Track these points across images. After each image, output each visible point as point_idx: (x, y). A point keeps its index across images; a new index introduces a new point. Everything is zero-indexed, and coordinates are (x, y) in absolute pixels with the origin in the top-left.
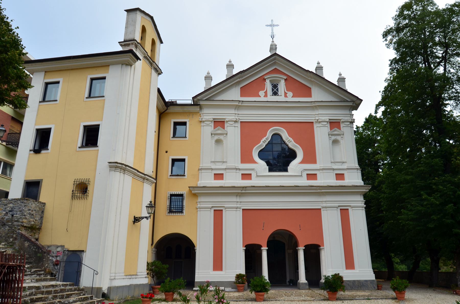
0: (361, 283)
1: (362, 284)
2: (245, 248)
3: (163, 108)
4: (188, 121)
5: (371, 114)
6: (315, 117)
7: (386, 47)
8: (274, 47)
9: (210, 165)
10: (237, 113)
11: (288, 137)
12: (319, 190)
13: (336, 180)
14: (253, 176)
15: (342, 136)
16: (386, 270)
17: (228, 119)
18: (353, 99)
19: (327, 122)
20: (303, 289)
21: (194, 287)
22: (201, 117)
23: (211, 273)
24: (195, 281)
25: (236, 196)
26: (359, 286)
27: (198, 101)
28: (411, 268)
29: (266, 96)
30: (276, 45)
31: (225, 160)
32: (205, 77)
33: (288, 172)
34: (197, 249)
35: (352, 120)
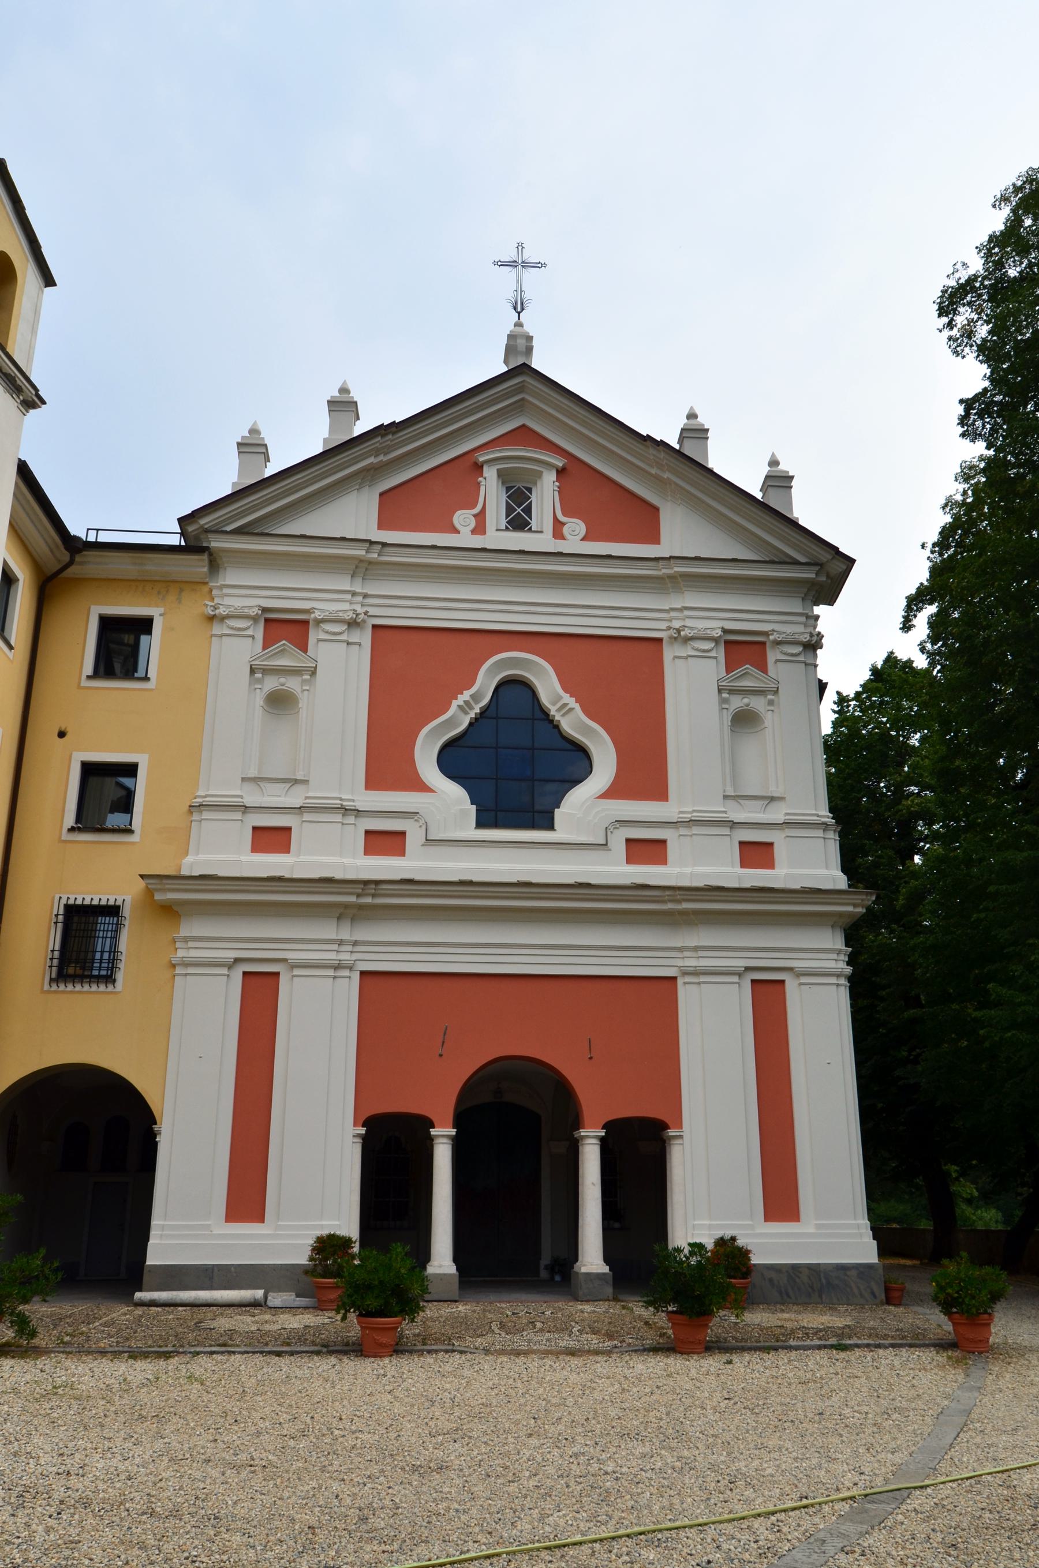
0: (822, 1275)
1: (824, 1281)
2: (362, 1131)
3: (54, 555)
4: (161, 615)
5: (892, 653)
6: (670, 620)
7: (949, 351)
8: (521, 343)
9: (238, 793)
10: (358, 590)
11: (558, 694)
12: (671, 901)
13: (741, 867)
14: (414, 839)
15: (770, 697)
16: (925, 1224)
17: (324, 611)
18: (820, 556)
19: (716, 640)
20: (589, 1298)
21: (140, 1290)
22: (212, 599)
23: (214, 1232)
24: (148, 1263)
25: (339, 918)
26: (812, 1288)
27: (202, 536)
28: (1017, 1219)
29: (480, 528)
30: (532, 337)
31: (301, 773)
32: (239, 444)
33: (555, 830)
34: (162, 1132)
35: (811, 635)
